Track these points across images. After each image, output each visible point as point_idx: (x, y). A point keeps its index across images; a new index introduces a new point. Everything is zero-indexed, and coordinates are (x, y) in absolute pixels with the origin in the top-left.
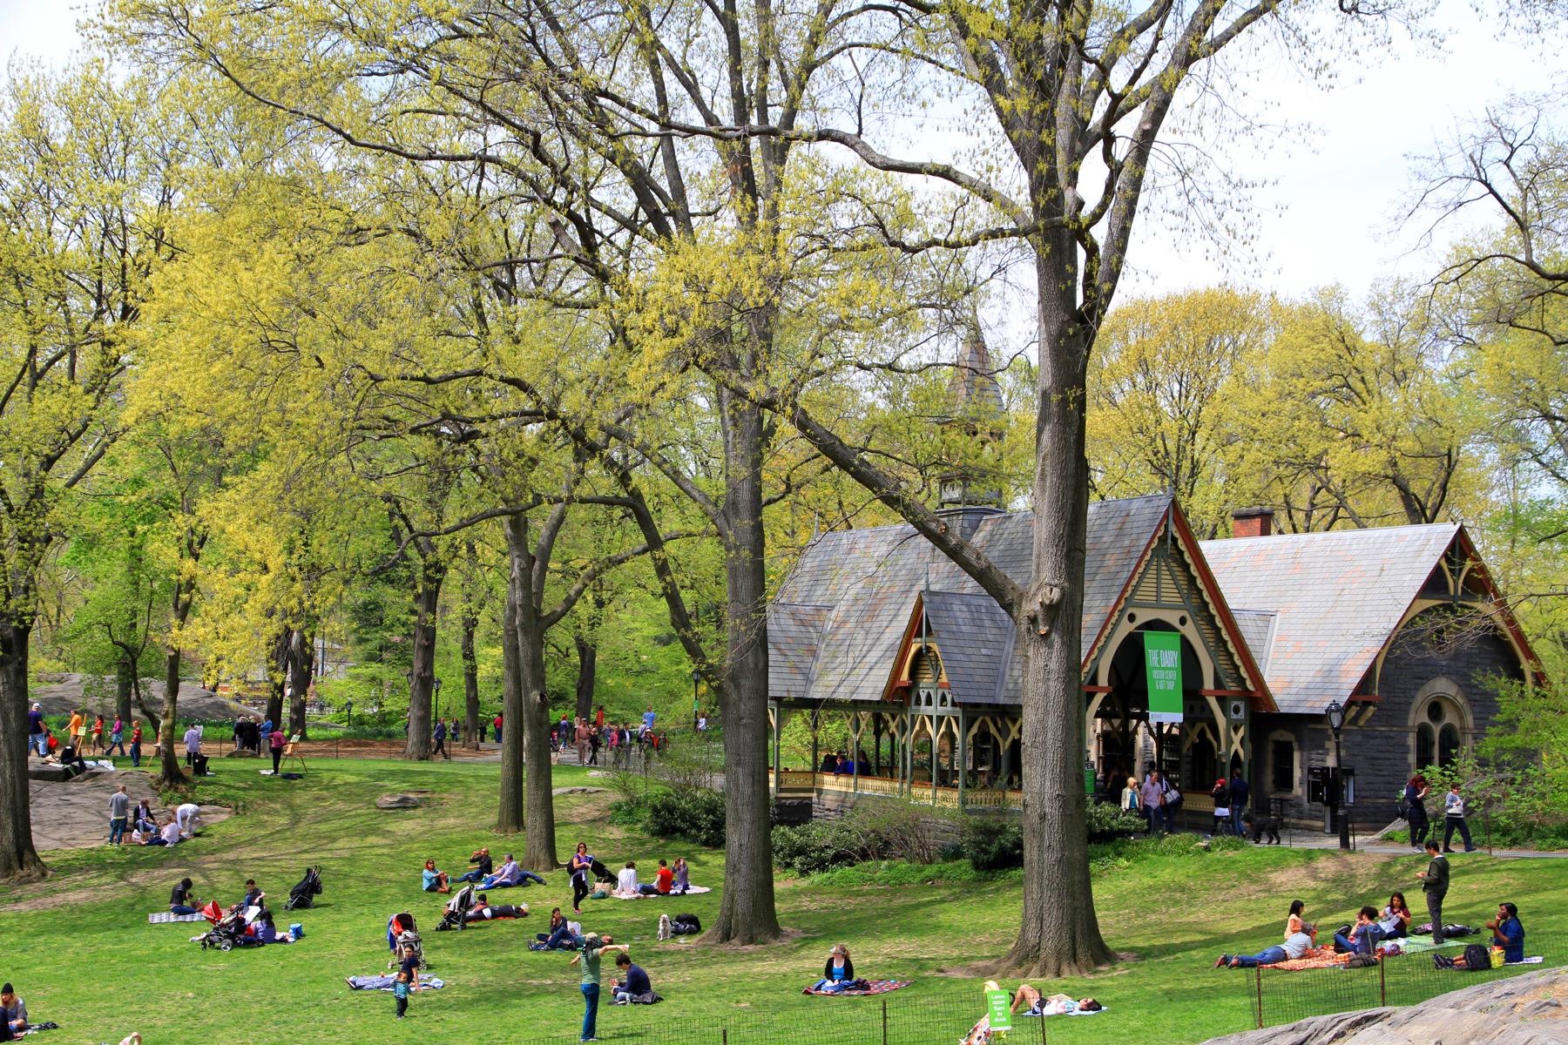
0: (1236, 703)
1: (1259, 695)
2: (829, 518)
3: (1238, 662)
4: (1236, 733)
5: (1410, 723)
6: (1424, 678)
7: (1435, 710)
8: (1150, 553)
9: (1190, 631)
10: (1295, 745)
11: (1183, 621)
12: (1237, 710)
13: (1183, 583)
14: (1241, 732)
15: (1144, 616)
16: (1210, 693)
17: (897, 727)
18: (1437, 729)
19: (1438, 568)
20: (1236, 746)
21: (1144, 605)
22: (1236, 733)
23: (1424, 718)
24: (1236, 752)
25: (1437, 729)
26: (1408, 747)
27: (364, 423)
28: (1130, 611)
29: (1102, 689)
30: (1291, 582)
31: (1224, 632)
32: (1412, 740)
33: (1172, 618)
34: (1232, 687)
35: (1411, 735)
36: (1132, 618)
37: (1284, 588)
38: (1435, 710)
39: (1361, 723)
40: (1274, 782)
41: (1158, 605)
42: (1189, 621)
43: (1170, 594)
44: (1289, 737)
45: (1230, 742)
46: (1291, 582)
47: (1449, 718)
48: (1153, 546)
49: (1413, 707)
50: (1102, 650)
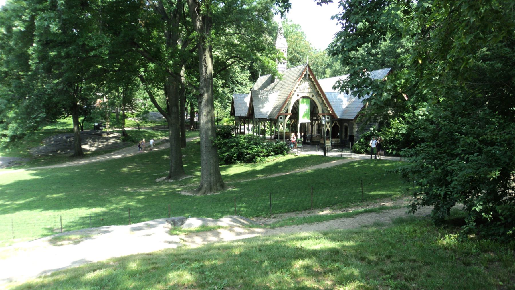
1: (333, 114)
3: (327, 106)
9: (315, 99)
11: (313, 96)
13: (67, 233)
16: (320, 114)
17: (280, 127)
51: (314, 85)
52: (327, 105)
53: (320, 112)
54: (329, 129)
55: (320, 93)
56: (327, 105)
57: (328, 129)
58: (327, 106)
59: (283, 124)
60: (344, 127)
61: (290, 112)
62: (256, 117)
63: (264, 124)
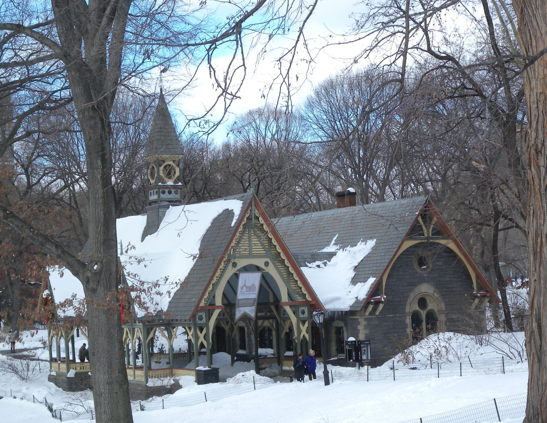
0: (303, 308)
1: (314, 303)
2: (192, 195)
3: (301, 285)
4: (201, 332)
5: (407, 310)
6: (414, 285)
7: (422, 302)
8: (241, 227)
9: (272, 270)
10: (345, 329)
11: (267, 264)
12: (303, 313)
13: (266, 242)
14: (307, 324)
15: (242, 263)
16: (286, 304)
17: (192, 335)
18: (423, 314)
19: (416, 220)
20: (304, 332)
21: (242, 257)
22: (201, 332)
23: (416, 307)
24: (304, 336)
25: (423, 314)
26: (407, 325)
27: (361, 25)
28: (233, 261)
29: (218, 307)
30: (348, 234)
31: (291, 269)
32: (408, 320)
33: (260, 263)
34: (300, 299)
35: (408, 317)
36: (234, 265)
37: (345, 238)
38: (422, 302)
39: (377, 313)
40: (337, 350)
41: (251, 255)
42: (271, 264)
43: (258, 249)
44: (341, 324)
45: (299, 332)
46: (348, 234)
47: (431, 306)
48: (244, 223)
49: (408, 302)
50: (215, 286)
51: (270, 240)
52: (299, 282)
53: (284, 298)
54: (307, 336)
55: (283, 256)
56: (299, 282)
57: (304, 336)
58: (301, 285)
59: (204, 331)
60: (333, 331)
61: (219, 301)
62: (216, 305)
63: (66, 88)
